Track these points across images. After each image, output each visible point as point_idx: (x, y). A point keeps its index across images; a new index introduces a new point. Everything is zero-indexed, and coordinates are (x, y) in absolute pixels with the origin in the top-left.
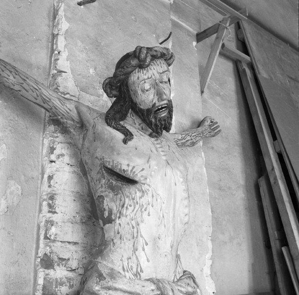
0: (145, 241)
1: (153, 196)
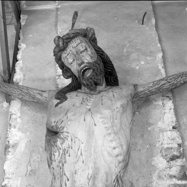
0: (67, 177)
1: (72, 140)
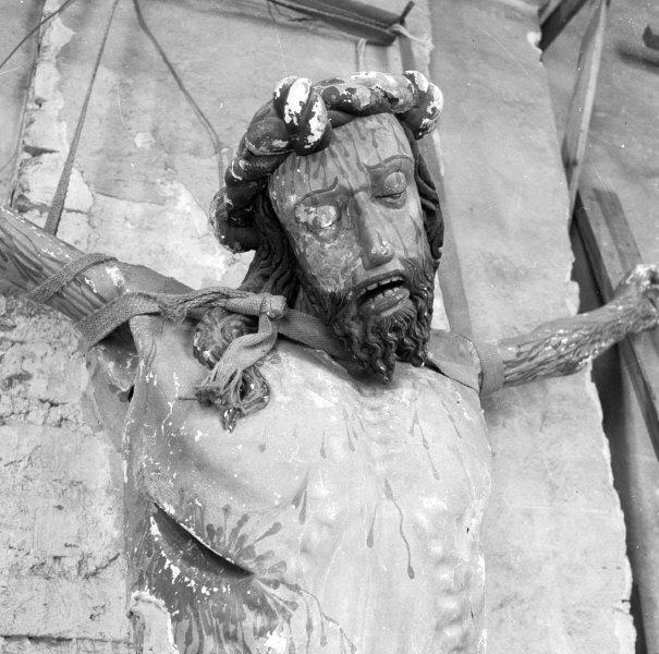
1: (309, 627)
